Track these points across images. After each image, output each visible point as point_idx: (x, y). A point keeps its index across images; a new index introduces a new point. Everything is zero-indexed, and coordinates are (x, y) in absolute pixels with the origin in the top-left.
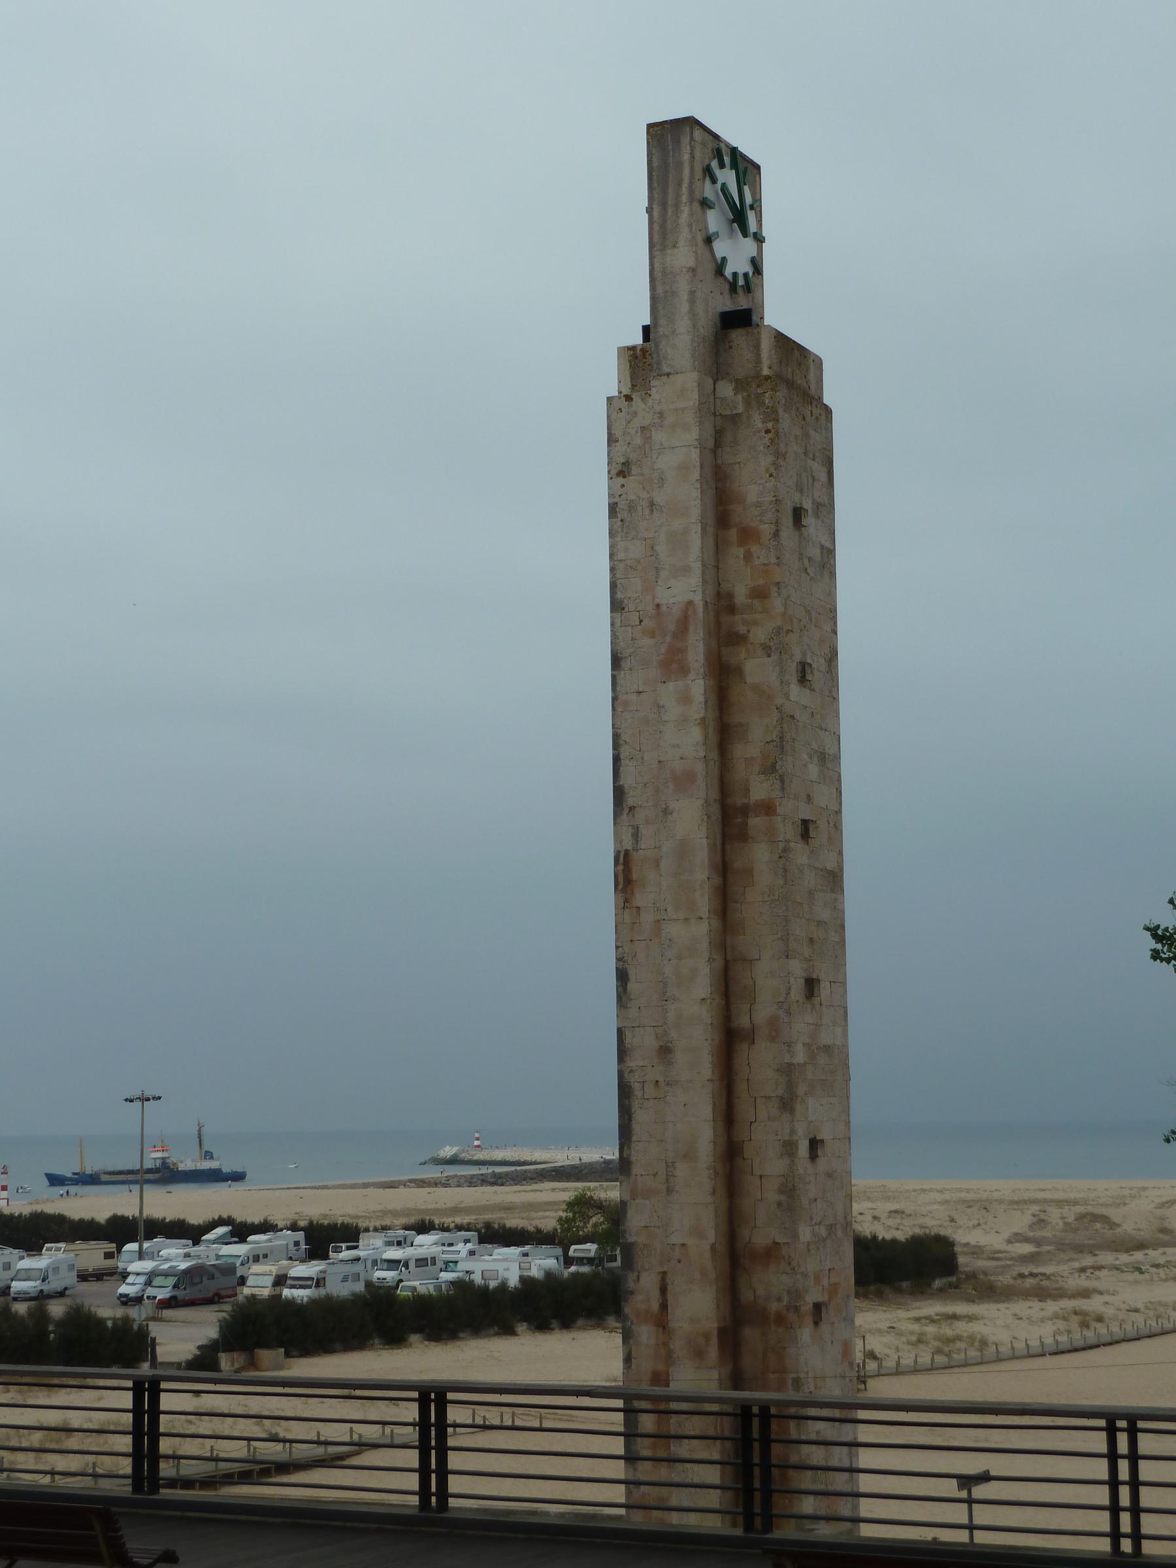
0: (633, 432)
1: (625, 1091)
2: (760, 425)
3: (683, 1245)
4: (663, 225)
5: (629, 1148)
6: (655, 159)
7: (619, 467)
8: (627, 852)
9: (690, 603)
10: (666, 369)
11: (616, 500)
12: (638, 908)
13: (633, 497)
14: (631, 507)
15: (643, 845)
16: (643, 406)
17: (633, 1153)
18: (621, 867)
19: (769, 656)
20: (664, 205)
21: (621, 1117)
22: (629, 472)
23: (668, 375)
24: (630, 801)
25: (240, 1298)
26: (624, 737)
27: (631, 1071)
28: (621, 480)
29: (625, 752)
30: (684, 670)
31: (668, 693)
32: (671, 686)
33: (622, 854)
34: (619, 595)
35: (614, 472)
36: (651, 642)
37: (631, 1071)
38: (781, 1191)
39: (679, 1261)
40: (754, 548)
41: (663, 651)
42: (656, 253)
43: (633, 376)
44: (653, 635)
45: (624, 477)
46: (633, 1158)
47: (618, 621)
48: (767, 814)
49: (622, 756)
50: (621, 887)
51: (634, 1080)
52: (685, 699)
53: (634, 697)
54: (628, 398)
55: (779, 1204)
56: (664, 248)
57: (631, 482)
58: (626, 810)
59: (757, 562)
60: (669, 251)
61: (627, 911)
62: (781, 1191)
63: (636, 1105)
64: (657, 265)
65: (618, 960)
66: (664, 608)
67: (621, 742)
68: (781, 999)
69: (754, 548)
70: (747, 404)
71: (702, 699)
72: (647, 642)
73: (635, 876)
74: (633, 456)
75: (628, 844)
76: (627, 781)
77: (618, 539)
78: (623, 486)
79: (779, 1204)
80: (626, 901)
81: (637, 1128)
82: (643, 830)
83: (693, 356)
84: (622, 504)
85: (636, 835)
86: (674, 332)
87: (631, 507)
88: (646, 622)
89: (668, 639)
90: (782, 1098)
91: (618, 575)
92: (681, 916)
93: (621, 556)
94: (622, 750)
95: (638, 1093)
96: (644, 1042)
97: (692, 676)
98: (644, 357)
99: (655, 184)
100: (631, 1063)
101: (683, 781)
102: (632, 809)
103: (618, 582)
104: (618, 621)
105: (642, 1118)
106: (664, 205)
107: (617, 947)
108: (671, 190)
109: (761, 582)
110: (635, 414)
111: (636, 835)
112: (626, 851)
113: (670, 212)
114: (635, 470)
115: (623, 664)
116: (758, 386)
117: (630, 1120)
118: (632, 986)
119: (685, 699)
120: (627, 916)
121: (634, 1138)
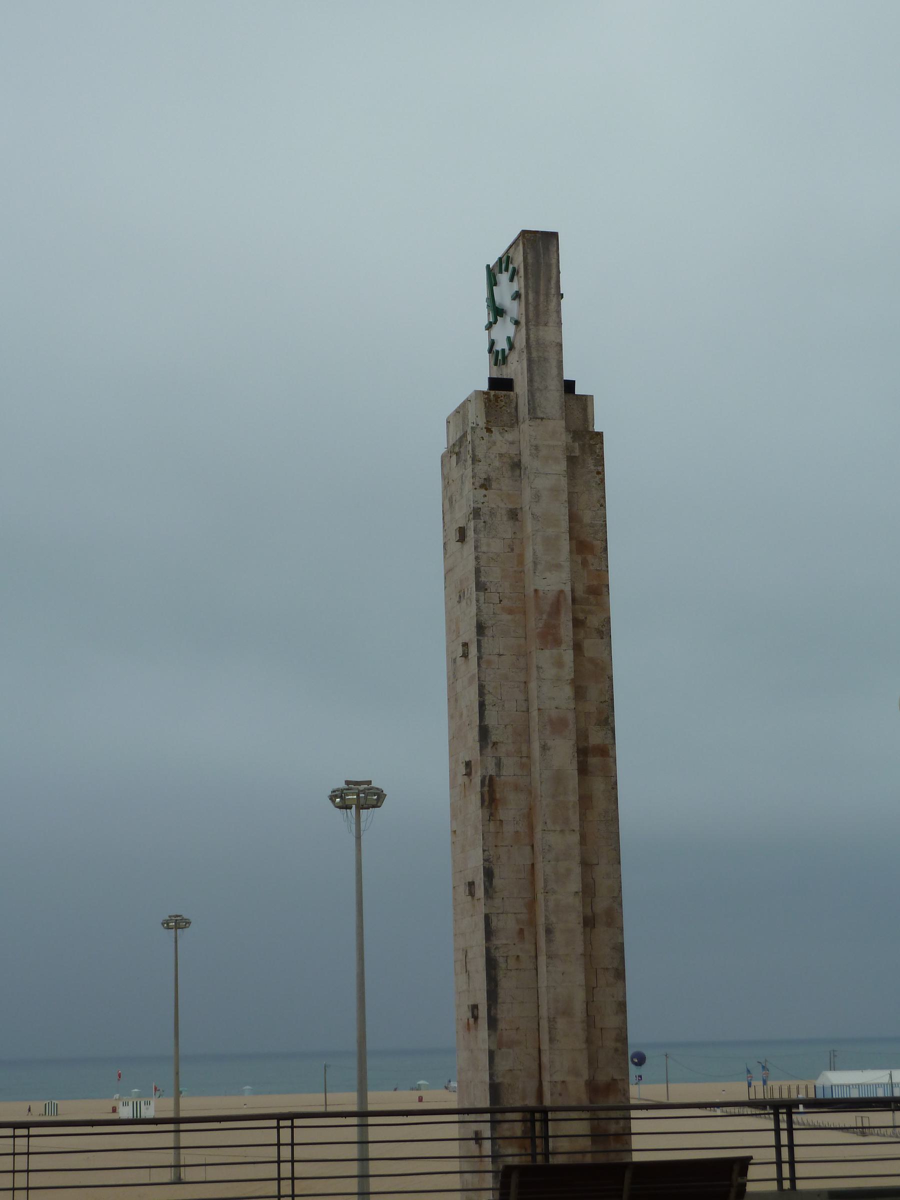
0: (493, 457)
1: (491, 964)
2: (592, 467)
3: (563, 1082)
4: (537, 307)
5: (496, 1009)
6: (529, 257)
7: (482, 481)
8: (491, 777)
9: (562, 592)
10: (541, 415)
11: (479, 506)
12: (501, 821)
13: (493, 506)
14: (492, 513)
15: (504, 772)
16: (501, 438)
17: (499, 1012)
18: (486, 789)
19: (602, 638)
20: (537, 293)
21: (488, 984)
22: (490, 486)
23: (542, 419)
24: (494, 738)
25: (819, 1082)
26: (488, 688)
27: (497, 948)
28: (483, 492)
29: (489, 699)
30: (557, 642)
31: (543, 658)
32: (547, 652)
33: (487, 778)
34: (483, 579)
35: (477, 484)
36: (509, 617)
37: (497, 948)
38: (617, 1040)
39: (560, 1095)
40: (590, 558)
41: (541, 625)
42: (531, 327)
43: (487, 414)
44: (511, 612)
45: (486, 489)
46: (499, 1016)
47: (482, 599)
48: (602, 756)
49: (486, 703)
50: (486, 803)
51: (499, 955)
52: (559, 664)
53: (495, 658)
54: (489, 430)
55: (616, 1050)
56: (537, 324)
57: (491, 493)
58: (490, 745)
59: (591, 568)
60: (541, 328)
61: (492, 823)
62: (617, 1040)
63: (501, 974)
64: (532, 336)
65: (485, 860)
66: (541, 593)
67: (486, 692)
68: (615, 895)
69: (590, 558)
70: (582, 448)
71: (572, 665)
72: (506, 617)
73: (498, 796)
74: (493, 475)
75: (492, 771)
76: (492, 719)
77: (482, 536)
78: (485, 496)
79: (616, 1050)
80: (491, 815)
81: (502, 994)
82: (504, 761)
83: (561, 408)
84: (485, 510)
85: (499, 764)
86: (546, 387)
87: (492, 513)
88: (505, 602)
89: (545, 617)
90: (617, 969)
91: (482, 563)
92: (558, 829)
93: (484, 548)
94: (486, 698)
95: (503, 965)
96: (507, 924)
97: (564, 646)
98: (497, 401)
99: (530, 276)
100: (496, 942)
101: (557, 725)
102: (495, 744)
103: (482, 568)
104: (482, 599)
105: (506, 984)
106: (537, 293)
107: (484, 851)
108: (542, 283)
109: (595, 583)
110: (495, 443)
111: (499, 764)
112: (491, 777)
113: (542, 298)
114: (494, 485)
115: (486, 632)
116: (591, 439)
117: (496, 986)
118: (497, 882)
119: (559, 664)
120: (492, 827)
121: (500, 1000)
